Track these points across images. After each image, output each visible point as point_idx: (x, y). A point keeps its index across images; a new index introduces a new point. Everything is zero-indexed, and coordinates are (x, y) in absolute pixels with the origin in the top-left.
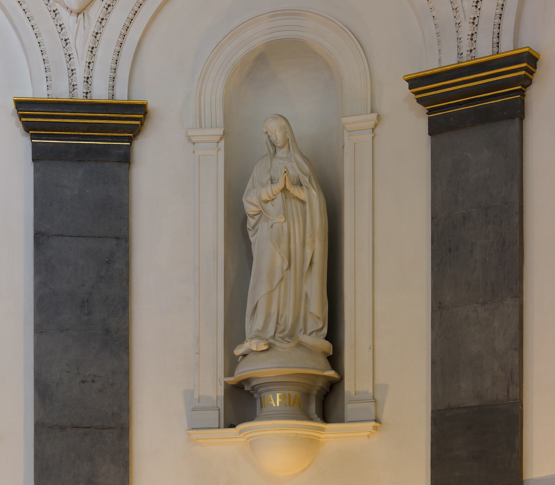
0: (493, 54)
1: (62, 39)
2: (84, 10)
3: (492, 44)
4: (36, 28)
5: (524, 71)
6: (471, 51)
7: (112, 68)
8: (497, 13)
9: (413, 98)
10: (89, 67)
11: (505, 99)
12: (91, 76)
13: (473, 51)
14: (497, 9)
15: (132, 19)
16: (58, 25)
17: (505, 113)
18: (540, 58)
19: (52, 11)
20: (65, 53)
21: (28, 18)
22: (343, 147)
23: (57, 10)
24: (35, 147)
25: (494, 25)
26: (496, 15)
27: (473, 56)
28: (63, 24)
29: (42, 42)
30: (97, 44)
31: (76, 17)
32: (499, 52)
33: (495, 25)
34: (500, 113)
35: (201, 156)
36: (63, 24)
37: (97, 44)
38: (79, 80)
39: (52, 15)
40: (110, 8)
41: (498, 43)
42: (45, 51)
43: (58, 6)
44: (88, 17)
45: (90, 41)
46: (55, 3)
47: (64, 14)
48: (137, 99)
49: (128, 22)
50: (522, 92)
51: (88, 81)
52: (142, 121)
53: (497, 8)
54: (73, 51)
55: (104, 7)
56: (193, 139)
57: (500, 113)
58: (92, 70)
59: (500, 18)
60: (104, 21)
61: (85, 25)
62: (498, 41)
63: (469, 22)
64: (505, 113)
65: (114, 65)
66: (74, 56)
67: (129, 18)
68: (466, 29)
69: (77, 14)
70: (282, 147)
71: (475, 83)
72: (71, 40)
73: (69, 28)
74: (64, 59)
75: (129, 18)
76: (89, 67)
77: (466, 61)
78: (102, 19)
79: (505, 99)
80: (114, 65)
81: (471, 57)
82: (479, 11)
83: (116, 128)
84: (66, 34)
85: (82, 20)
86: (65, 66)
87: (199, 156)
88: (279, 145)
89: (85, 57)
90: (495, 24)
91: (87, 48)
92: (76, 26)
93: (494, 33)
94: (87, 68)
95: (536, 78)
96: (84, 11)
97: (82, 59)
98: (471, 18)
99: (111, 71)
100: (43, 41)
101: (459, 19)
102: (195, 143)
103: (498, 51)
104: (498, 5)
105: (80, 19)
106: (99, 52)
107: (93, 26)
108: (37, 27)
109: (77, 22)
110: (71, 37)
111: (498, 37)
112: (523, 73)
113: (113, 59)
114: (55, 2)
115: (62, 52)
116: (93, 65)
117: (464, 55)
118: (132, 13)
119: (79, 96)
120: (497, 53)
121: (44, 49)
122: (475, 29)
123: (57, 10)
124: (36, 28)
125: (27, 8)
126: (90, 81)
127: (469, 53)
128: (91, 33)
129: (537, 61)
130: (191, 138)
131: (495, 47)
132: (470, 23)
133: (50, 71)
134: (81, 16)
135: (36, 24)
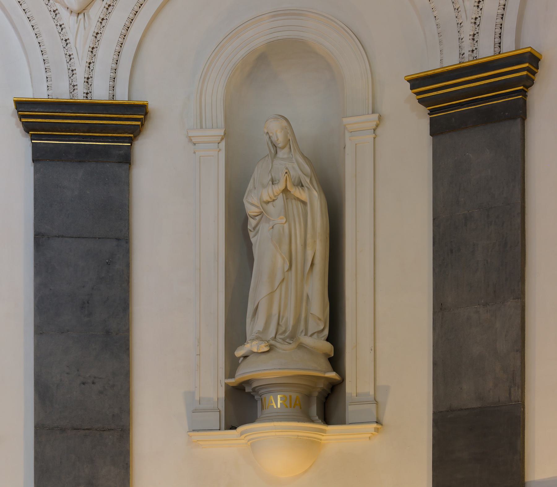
0: (495, 54)
1: (62, 39)
2: (84, 10)
3: (494, 44)
4: (36, 28)
5: (526, 71)
6: (473, 51)
7: (112, 68)
8: (499, 13)
10: (89, 67)
11: (507, 99)
12: (92, 77)
13: (475, 51)
14: (498, 9)
15: (133, 20)
16: (59, 25)
17: (507, 113)
18: (542, 58)
19: (52, 11)
20: (66, 54)
21: (28, 18)
23: (57, 10)
24: (35, 148)
25: (496, 25)
26: (498, 15)
27: (475, 57)
28: (63, 24)
29: (42, 42)
30: (97, 44)
31: (76, 17)
32: (501, 53)
33: (497, 25)
34: (502, 113)
35: (202, 156)
36: (63, 24)
37: (97, 44)
38: (80, 80)
39: (52, 15)
40: (110, 8)
41: (500, 43)
42: (46, 51)
43: (58, 6)
44: (89, 17)
45: (90, 42)
46: (55, 3)
47: (64, 14)
48: (137, 99)
49: (129, 22)
50: (524, 93)
51: (88, 81)
52: (143, 122)
53: (499, 8)
54: (73, 52)
55: (105, 7)
57: (502, 113)
58: (93, 71)
59: (502, 18)
60: (105, 21)
61: (86, 25)
62: (500, 42)
63: (471, 22)
64: (507, 113)
65: (114, 66)
66: (74, 56)
67: (130, 18)
68: (468, 29)
69: (77, 14)
70: (283, 148)
71: (477, 83)
72: (71, 40)
73: (70, 28)
74: (64, 59)
75: (130, 18)
76: (89, 67)
77: (468, 61)
78: (103, 19)
79: (507, 99)
80: (114, 66)
81: (473, 57)
82: (481, 11)
83: (116, 129)
84: (66, 34)
85: (82, 20)
86: (65, 66)
88: (280, 145)
89: (86, 57)
90: (496, 24)
91: (87, 48)
92: (76, 26)
93: (496, 33)
94: (87, 68)
95: (538, 78)
96: (84, 11)
97: (82, 59)
98: (472, 18)
99: (111, 71)
100: (43, 41)
103: (500, 51)
104: (499, 5)
105: (81, 19)
106: (100, 52)
107: (94, 26)
108: (37, 27)
109: (77, 23)
110: (71, 37)
111: (500, 37)
112: (525, 73)
113: (113, 59)
114: (56, 2)
115: (63, 52)
116: (94, 65)
117: (466, 55)
118: (133, 13)
119: (80, 97)
121: (44, 49)
122: (477, 29)
123: (57, 10)
124: (36, 28)
125: (27, 8)
126: (90, 81)
127: (470, 53)
128: (91, 33)
129: (539, 61)
131: (496, 47)
132: (472, 23)
133: (50, 71)
134: (81, 16)
135: (36, 24)
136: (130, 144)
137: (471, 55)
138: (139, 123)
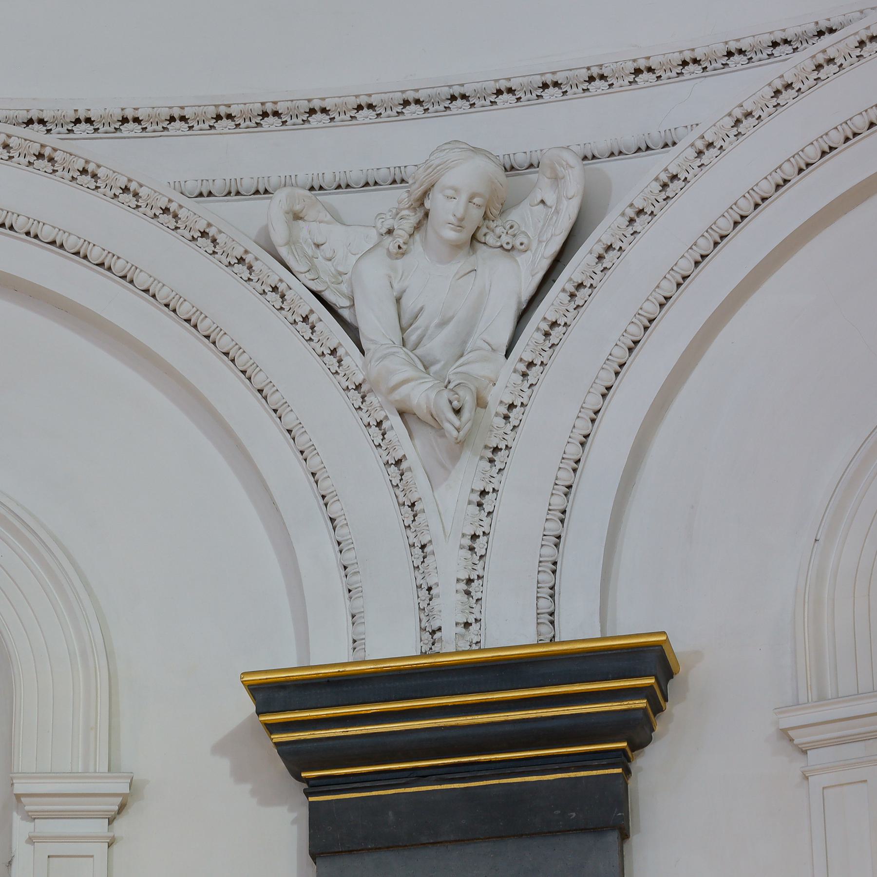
0: (539, 642)
3: (535, 614)
5: (643, 699)
6: (467, 625)
8: (550, 530)
9: (267, 744)
11: (572, 775)
12: (487, 532)
13: (474, 627)
14: (547, 520)
17: (574, 814)
18: (678, 672)
22: (10, 863)
25: (540, 562)
26: (545, 535)
27: (474, 641)
32: (557, 640)
33: (543, 564)
34: (558, 812)
35: (34, 826)
40: (556, 333)
41: (552, 614)
50: (622, 759)
51: (475, 546)
53: (548, 517)
56: (800, 738)
57: (558, 812)
59: (557, 545)
62: (551, 609)
63: (460, 545)
64: (574, 814)
71: (480, 717)
79: (572, 775)
81: (469, 643)
82: (489, 518)
87: (824, 788)
90: (541, 559)
93: (539, 585)
98: (463, 535)
101: (425, 532)
102: (806, 750)
103: (554, 637)
104: (549, 510)
111: (552, 596)
112: (641, 703)
120: (551, 641)
122: (479, 567)
126: (481, 546)
127: (461, 629)
129: (670, 679)
130: (791, 733)
131: (543, 623)
132: (462, 547)
136: (619, 770)
137: (463, 636)
138: (641, 703)
